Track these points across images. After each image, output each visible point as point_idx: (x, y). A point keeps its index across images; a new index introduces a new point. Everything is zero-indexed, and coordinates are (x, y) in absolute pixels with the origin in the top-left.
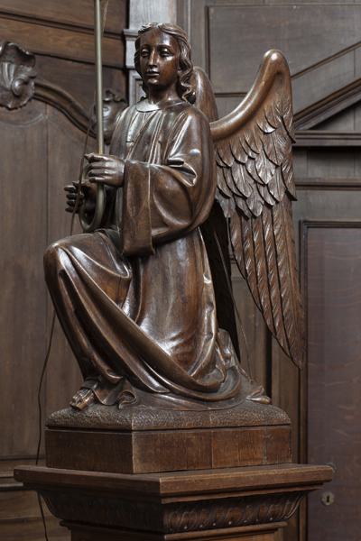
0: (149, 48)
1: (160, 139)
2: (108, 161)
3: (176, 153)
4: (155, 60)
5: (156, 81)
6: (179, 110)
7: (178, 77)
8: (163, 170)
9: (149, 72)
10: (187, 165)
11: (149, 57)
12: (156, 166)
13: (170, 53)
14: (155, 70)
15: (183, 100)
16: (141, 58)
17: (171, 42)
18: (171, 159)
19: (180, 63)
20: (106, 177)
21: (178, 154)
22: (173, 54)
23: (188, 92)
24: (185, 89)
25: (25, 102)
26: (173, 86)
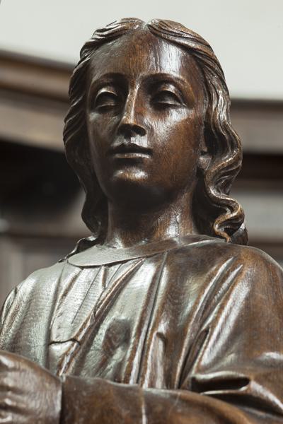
0: (121, 83)
1: (162, 328)
2: (14, 369)
3: (218, 359)
4: (139, 114)
5: (139, 175)
6: (200, 263)
7: (200, 173)
8: (185, 401)
9: (123, 149)
10: (256, 387)
11: (120, 108)
12: (160, 389)
13: (183, 99)
14: (141, 141)
15: (216, 235)
16: (93, 116)
17: (185, 69)
18: (201, 377)
19: (207, 124)
20: (74, 251)
21: (230, 358)
22: (190, 104)
23: (230, 215)
24: (221, 207)
25: (47, 397)
26: (185, 199)
